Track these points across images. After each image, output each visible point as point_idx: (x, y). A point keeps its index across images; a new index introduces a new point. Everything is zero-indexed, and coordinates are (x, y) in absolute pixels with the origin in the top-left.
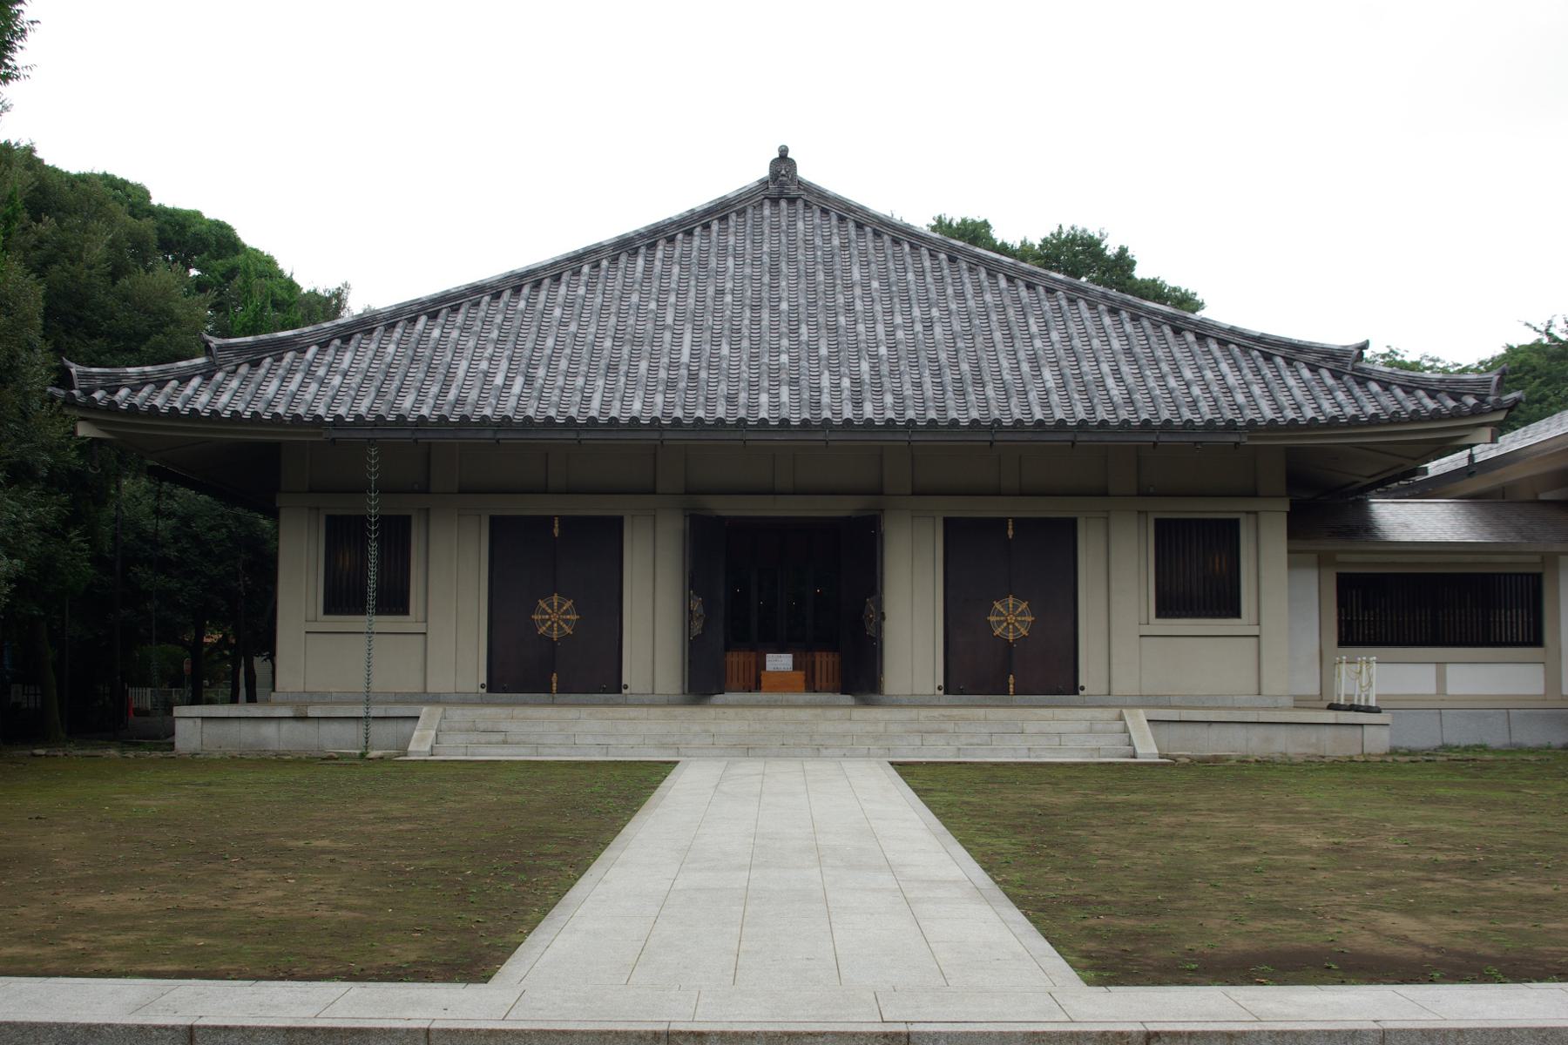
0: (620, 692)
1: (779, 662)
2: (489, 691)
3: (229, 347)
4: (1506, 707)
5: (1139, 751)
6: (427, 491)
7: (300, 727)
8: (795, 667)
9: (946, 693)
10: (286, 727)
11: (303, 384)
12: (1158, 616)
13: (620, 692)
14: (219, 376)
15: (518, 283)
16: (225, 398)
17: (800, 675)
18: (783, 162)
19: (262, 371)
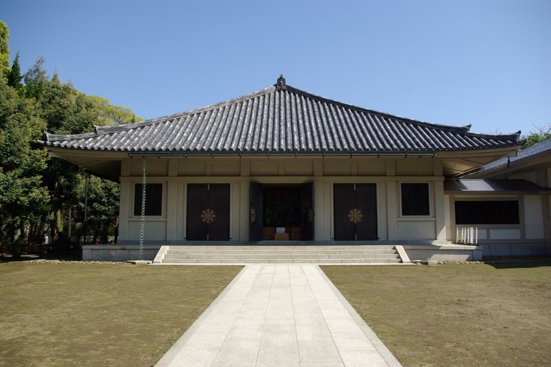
0: (229, 240)
1: (281, 230)
2: (187, 240)
3: (102, 129)
4: (509, 243)
5: (404, 260)
6: (167, 176)
7: (123, 252)
8: (286, 232)
9: (335, 240)
10: (119, 252)
11: (125, 141)
12: (403, 215)
13: (229, 240)
14: (99, 138)
15: (199, 112)
16: (98, 144)
17: (287, 234)
18: (281, 79)
19: (113, 136)
